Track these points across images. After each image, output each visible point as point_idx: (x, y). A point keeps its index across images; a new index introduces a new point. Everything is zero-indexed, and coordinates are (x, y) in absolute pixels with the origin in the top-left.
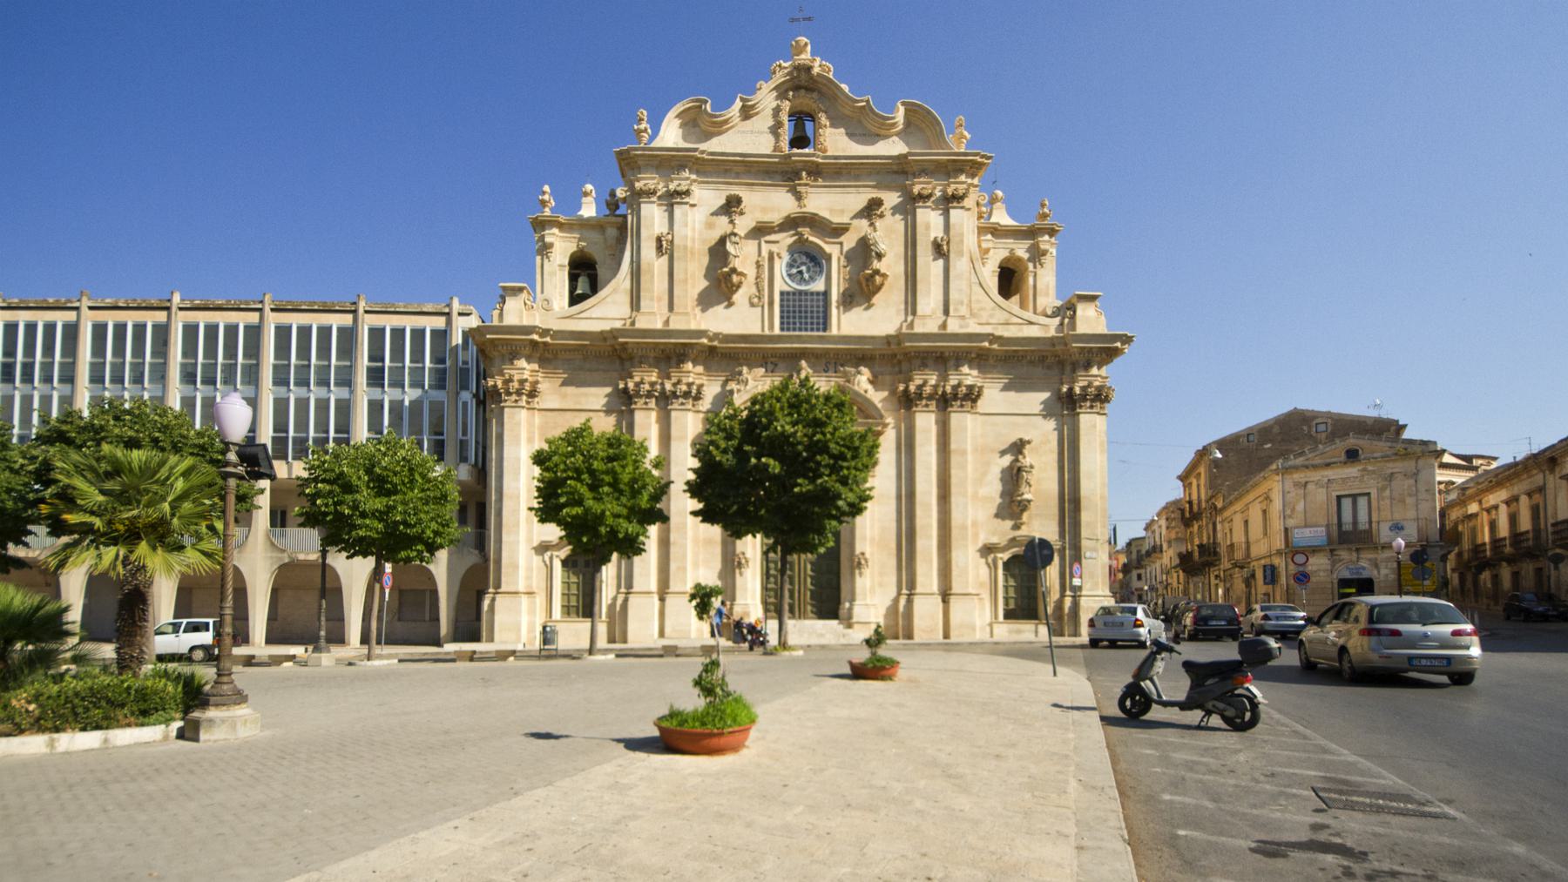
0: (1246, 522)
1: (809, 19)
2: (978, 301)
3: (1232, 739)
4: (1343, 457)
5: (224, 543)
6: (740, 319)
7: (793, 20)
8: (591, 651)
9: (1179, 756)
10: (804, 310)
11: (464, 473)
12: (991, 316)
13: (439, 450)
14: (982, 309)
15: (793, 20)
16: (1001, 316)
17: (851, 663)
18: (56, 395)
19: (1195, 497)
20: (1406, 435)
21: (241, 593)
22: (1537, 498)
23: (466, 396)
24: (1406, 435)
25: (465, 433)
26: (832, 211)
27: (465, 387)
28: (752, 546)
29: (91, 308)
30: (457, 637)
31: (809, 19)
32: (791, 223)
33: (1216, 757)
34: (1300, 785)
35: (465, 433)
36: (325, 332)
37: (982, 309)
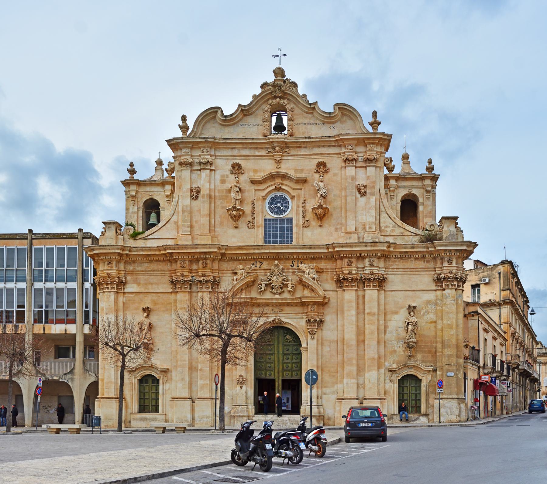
0: (198, 399)
1: (285, 55)
2: (385, 222)
3: (243, 175)
4: (264, 376)
5: (235, 259)
6: (250, 237)
7: (274, 56)
8: (510, 290)
9: (10, 466)
10: (278, 231)
11: (87, 329)
12: (393, 231)
13: (475, 287)
14: (387, 227)
15: (274, 56)
16: (398, 231)
17: (279, 72)
18: (72, 329)
19: (212, 187)
20: (173, 155)
21: (19, 397)
22: (61, 304)
23: (87, 285)
24: (173, 155)
25: (87, 307)
26: (296, 170)
27: (86, 280)
28: (482, 392)
29: (385, 335)
30: (12, 290)
31: (285, 55)
32: (272, 177)
33: (50, 428)
34: (214, 248)
35: (87, 307)
36: (61, 251)
37: (387, 227)
